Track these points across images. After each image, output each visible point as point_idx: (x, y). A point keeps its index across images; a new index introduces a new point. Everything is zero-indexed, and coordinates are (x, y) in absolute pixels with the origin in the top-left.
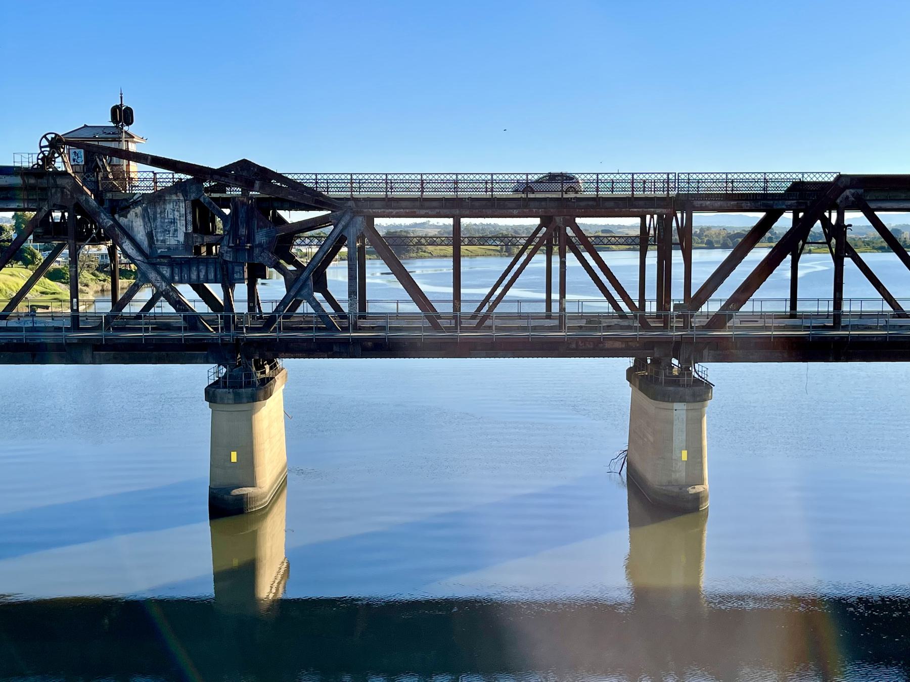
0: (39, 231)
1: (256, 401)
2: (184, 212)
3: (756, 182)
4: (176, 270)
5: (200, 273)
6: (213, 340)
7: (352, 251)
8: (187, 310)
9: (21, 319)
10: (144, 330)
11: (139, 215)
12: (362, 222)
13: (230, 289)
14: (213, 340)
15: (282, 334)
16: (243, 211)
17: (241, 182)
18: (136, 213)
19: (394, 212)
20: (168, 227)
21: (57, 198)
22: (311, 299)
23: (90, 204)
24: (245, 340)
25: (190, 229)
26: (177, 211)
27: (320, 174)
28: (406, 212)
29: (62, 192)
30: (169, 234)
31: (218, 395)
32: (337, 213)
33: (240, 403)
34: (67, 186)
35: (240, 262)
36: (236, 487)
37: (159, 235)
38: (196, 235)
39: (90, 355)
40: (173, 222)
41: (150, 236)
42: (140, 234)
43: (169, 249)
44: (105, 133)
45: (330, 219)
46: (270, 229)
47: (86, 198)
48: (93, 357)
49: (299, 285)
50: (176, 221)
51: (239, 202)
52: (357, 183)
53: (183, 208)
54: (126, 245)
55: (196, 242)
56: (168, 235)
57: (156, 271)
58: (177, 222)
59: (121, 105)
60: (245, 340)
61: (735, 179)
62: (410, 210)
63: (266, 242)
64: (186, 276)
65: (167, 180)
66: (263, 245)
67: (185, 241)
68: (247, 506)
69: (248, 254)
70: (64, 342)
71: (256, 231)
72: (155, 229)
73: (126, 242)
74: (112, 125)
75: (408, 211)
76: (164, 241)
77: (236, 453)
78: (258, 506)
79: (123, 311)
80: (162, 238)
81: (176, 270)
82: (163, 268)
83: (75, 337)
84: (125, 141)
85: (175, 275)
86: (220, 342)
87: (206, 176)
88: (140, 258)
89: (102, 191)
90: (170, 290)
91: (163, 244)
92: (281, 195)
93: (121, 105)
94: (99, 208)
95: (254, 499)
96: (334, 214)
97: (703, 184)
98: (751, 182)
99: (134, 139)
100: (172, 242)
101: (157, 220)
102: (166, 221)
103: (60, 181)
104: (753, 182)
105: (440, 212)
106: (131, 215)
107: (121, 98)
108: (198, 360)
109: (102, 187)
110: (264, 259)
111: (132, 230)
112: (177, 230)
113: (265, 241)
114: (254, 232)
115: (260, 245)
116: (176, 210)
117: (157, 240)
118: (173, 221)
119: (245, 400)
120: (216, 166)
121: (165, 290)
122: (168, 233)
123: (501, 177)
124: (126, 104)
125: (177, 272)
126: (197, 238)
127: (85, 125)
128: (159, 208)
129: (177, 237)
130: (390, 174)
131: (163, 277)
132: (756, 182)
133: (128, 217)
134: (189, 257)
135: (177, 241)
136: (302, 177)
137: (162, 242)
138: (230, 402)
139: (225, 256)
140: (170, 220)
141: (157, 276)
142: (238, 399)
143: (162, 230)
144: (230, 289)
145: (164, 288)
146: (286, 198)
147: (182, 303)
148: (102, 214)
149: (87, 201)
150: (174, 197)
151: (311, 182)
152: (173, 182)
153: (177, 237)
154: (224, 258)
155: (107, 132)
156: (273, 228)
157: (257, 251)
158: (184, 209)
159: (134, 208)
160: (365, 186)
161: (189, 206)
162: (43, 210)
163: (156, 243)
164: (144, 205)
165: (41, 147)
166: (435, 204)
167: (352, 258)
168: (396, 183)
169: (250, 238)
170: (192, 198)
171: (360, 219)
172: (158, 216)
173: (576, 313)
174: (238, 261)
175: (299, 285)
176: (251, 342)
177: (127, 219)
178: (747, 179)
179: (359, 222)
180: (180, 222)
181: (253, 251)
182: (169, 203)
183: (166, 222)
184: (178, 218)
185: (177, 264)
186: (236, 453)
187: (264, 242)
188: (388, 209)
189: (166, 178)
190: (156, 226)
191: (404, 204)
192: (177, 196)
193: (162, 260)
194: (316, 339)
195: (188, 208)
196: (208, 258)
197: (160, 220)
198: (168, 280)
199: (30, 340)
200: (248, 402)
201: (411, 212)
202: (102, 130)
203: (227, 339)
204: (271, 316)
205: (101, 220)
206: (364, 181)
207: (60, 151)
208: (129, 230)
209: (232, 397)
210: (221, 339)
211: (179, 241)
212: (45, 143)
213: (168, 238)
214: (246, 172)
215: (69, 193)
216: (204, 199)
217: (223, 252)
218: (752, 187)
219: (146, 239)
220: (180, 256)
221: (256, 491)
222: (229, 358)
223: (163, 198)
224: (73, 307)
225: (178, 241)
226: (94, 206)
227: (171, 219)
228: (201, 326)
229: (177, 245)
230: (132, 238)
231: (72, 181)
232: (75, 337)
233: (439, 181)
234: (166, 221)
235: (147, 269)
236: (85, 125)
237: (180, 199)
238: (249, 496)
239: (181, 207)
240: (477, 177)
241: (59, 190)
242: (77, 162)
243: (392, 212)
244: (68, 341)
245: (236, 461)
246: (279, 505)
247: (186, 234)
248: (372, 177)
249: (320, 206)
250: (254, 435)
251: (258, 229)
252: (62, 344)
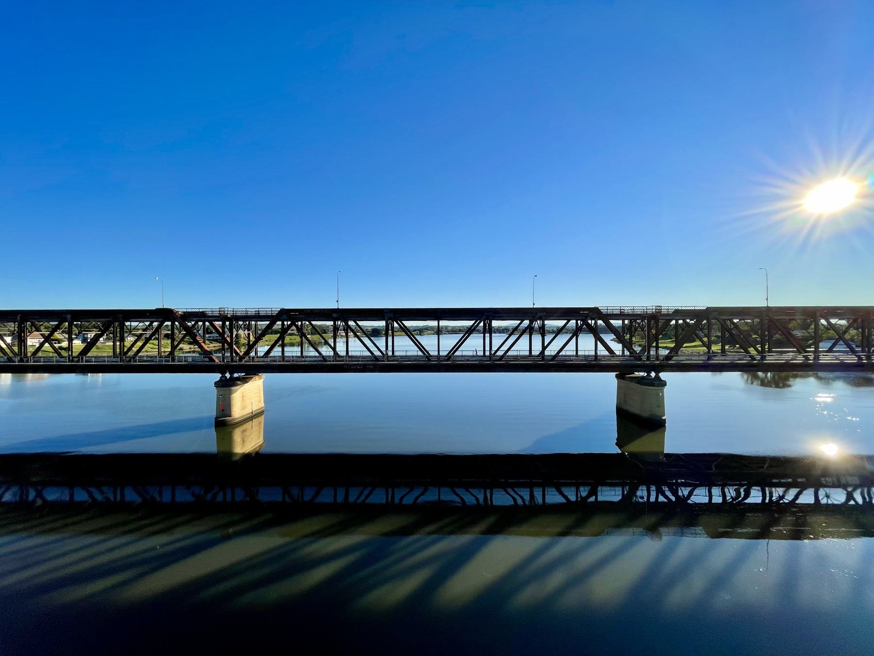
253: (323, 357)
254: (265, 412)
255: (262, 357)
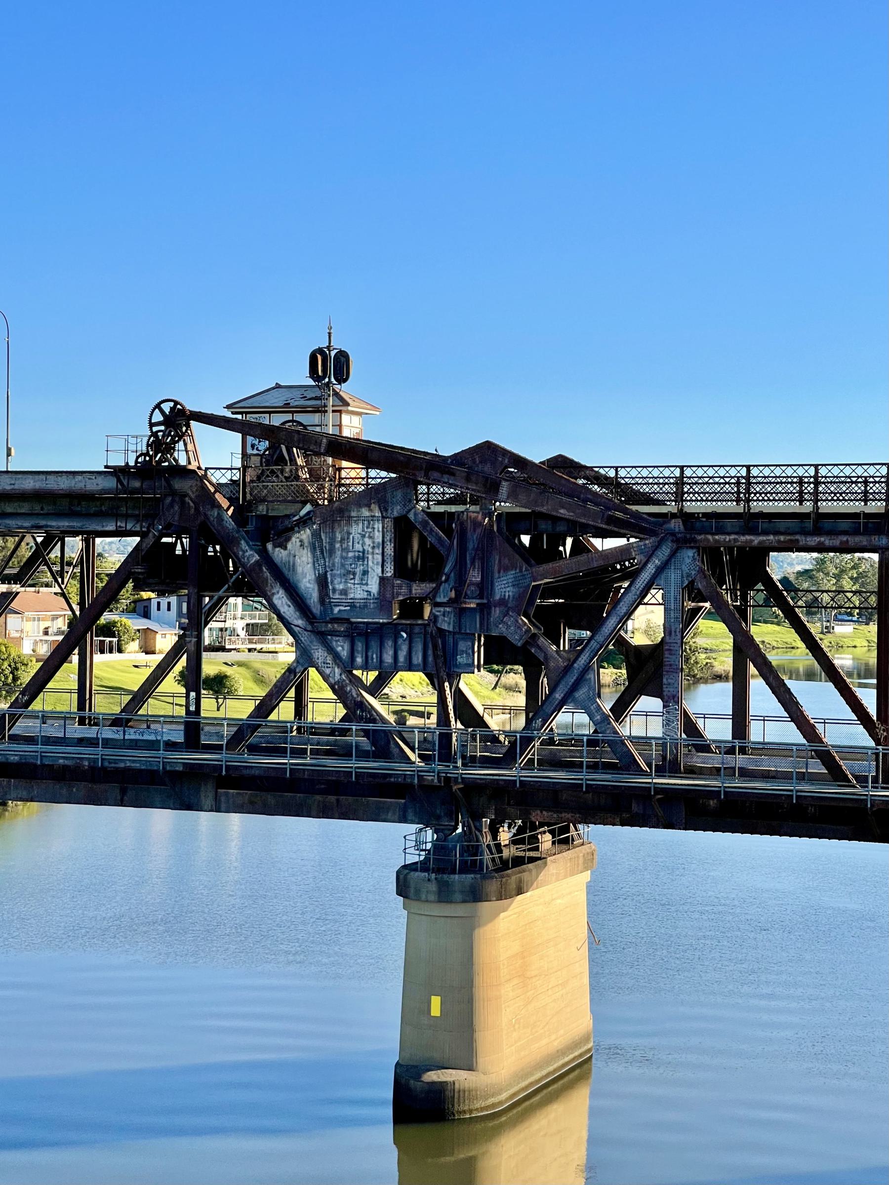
0: (140, 570)
1: (481, 901)
2: (380, 540)
3: (852, 482)
4: (359, 646)
5: (399, 652)
6: (405, 779)
7: (672, 615)
8: (374, 721)
9: (152, 726)
10: (291, 753)
11: (306, 544)
12: (694, 559)
13: (446, 684)
14: (405, 779)
15: (536, 773)
16: (475, 538)
17: (476, 484)
18: (301, 541)
19: (756, 542)
20: (353, 566)
21: (174, 515)
22: (592, 708)
23: (225, 522)
24: (460, 780)
25: (390, 572)
26: (370, 537)
27: (624, 467)
28: (779, 541)
29: (183, 504)
30: (354, 578)
31: (412, 882)
32: (647, 542)
33: (447, 902)
34: (191, 493)
35: (467, 634)
36: (438, 1067)
37: (338, 580)
38: (399, 582)
39: (211, 795)
40: (362, 557)
41: (322, 582)
42: (307, 582)
43: (352, 606)
44: (305, 397)
45: (633, 554)
46: (521, 571)
47: (218, 514)
48: (217, 798)
49: (571, 679)
50: (366, 555)
51: (469, 521)
52: (671, 483)
53: (378, 531)
54: (279, 598)
55: (398, 594)
56: (352, 581)
57: (325, 647)
58: (368, 558)
59: (328, 347)
60: (460, 780)
61: (870, 477)
62: (788, 538)
63: (514, 596)
64: (374, 656)
65: (357, 481)
66: (508, 601)
67: (379, 593)
68: (453, 1106)
69: (480, 617)
70: (161, 768)
71: (496, 575)
72: (332, 570)
73: (278, 592)
74: (311, 382)
75: (782, 538)
76: (344, 592)
77: (439, 998)
78: (477, 1109)
79: (270, 718)
80: (341, 587)
81: (359, 646)
82: (337, 641)
83: (179, 761)
84: (334, 411)
85: (356, 654)
86: (416, 781)
87: (417, 473)
88: (300, 622)
89: (250, 500)
90: (347, 682)
91: (343, 597)
92: (545, 508)
93: (328, 347)
94: (238, 532)
95: (468, 1094)
96: (642, 543)
97: (854, 485)
98: (842, 482)
99: (350, 408)
100: (358, 593)
101: (335, 553)
102: (351, 554)
103: (179, 484)
104: (846, 482)
105: (847, 541)
106: (294, 542)
107: (330, 334)
108: (390, 814)
109: (251, 494)
110: (508, 627)
111: (293, 570)
112: (368, 572)
113: (510, 593)
114: (492, 577)
115: (503, 602)
116: (367, 535)
117: (334, 590)
118: (361, 554)
119: (458, 896)
120: (447, 451)
121: (338, 681)
122: (352, 577)
123: (836, 471)
124: (338, 344)
125: (360, 649)
126: (400, 587)
127: (277, 384)
128: (340, 532)
129: (367, 584)
130: (624, 467)
131: (336, 657)
132: (852, 482)
133: (288, 548)
134: (381, 621)
135: (367, 591)
136: (634, 473)
137: (341, 594)
138: (432, 897)
139: (440, 621)
140: (357, 554)
141: (326, 654)
142: (444, 895)
143: (343, 571)
144: (446, 684)
145: (337, 677)
146: (554, 514)
147: (366, 706)
148: (243, 542)
149: (220, 518)
150: (365, 512)
151: (717, 483)
152: (368, 484)
153: (367, 584)
154: (439, 626)
155: (309, 397)
156: (526, 570)
157: (496, 612)
158: (381, 533)
159: (299, 532)
160: (697, 490)
161: (389, 528)
162: (151, 535)
163: (331, 596)
164: (314, 527)
165: (152, 425)
166: (844, 524)
167: (673, 630)
168: (777, 483)
169: (485, 588)
170: (396, 514)
171: (690, 553)
172: (338, 545)
173: (759, 743)
174: (463, 631)
175: (571, 679)
176: (473, 787)
177: (286, 552)
178: (834, 477)
179: (688, 561)
180: (373, 558)
181: (489, 614)
182: (357, 522)
183: (351, 558)
184: (370, 550)
185: (359, 634)
186: (439, 998)
187: (509, 596)
188: (743, 534)
189: (356, 478)
190: (333, 565)
191: (782, 524)
192: (370, 510)
193: (336, 625)
194: (587, 785)
195: (387, 531)
196: (414, 625)
197: (340, 552)
198: (343, 664)
199: (110, 763)
200: (464, 901)
201: (791, 540)
202: (303, 392)
203: (430, 778)
204: (116, 718)
205: (241, 553)
206: (707, 480)
207: (181, 431)
208: (289, 571)
209: (434, 889)
210: (418, 776)
211: (370, 592)
212: (158, 417)
213: (352, 586)
214: (489, 465)
215: (192, 504)
216: (416, 514)
217: (438, 613)
218: (844, 492)
219: (316, 588)
220: (366, 620)
221: (474, 1078)
222: (442, 814)
223: (346, 514)
224: (189, 708)
225: (369, 592)
226: (231, 527)
227: (359, 552)
228: (395, 751)
229: (367, 599)
230: (292, 587)
231: (199, 483)
232: (179, 761)
233: (877, 479)
234: (351, 554)
235: (311, 642)
236: (277, 384)
237: (374, 516)
238: (457, 1086)
239: (376, 530)
240: (848, 471)
241: (177, 499)
242: (257, 449)
243: (752, 541)
244: (168, 768)
245: (439, 1015)
246: (552, 1116)
247: (383, 580)
248: (711, 472)
249: (616, 529)
250: (476, 967)
251: (499, 572)
252: (157, 771)
253: (826, 757)
254: (597, 1064)
255: (116, 722)
